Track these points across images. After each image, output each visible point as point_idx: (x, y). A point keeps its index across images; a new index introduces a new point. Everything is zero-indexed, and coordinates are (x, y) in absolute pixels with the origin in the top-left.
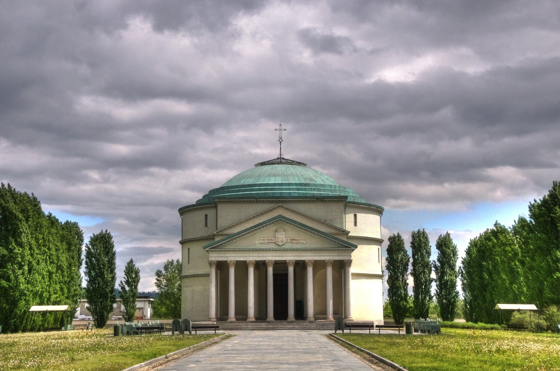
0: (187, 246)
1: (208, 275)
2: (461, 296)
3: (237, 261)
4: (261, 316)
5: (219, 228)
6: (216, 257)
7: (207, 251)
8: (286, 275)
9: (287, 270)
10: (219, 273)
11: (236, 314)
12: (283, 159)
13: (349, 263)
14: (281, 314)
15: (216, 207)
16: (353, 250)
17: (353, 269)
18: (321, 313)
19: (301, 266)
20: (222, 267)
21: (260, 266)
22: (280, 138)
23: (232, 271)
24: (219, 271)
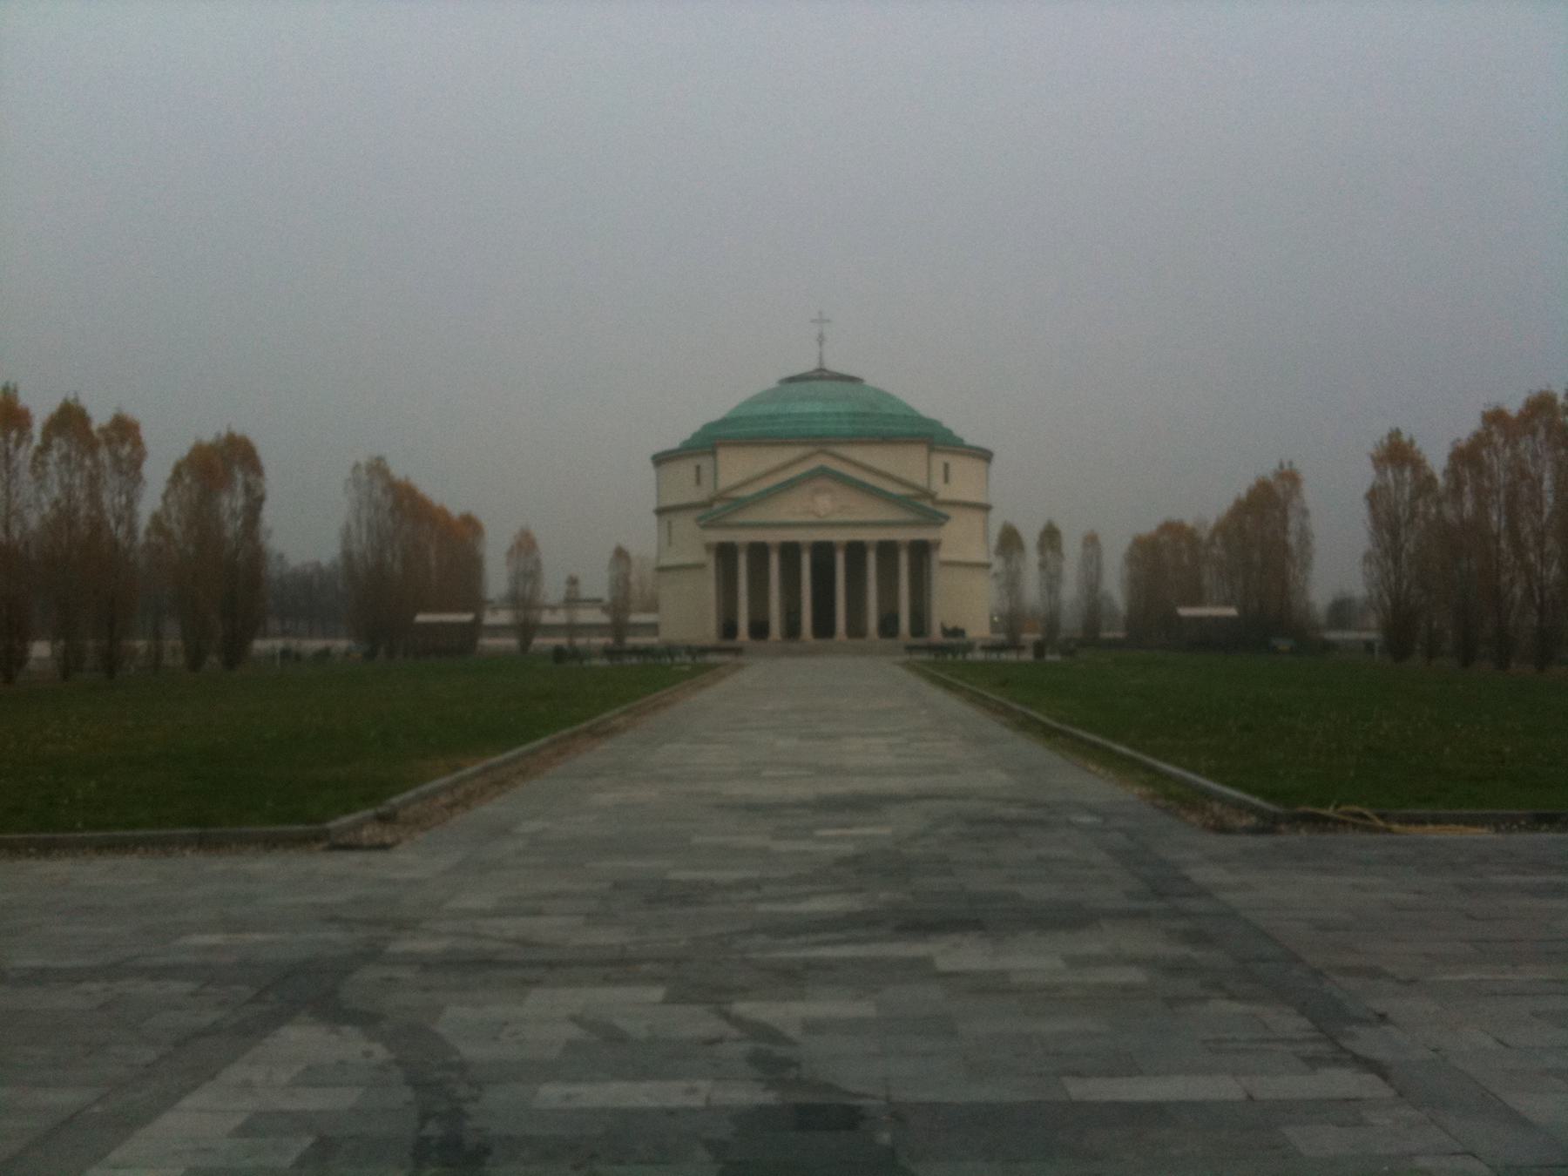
21: (790, 552)
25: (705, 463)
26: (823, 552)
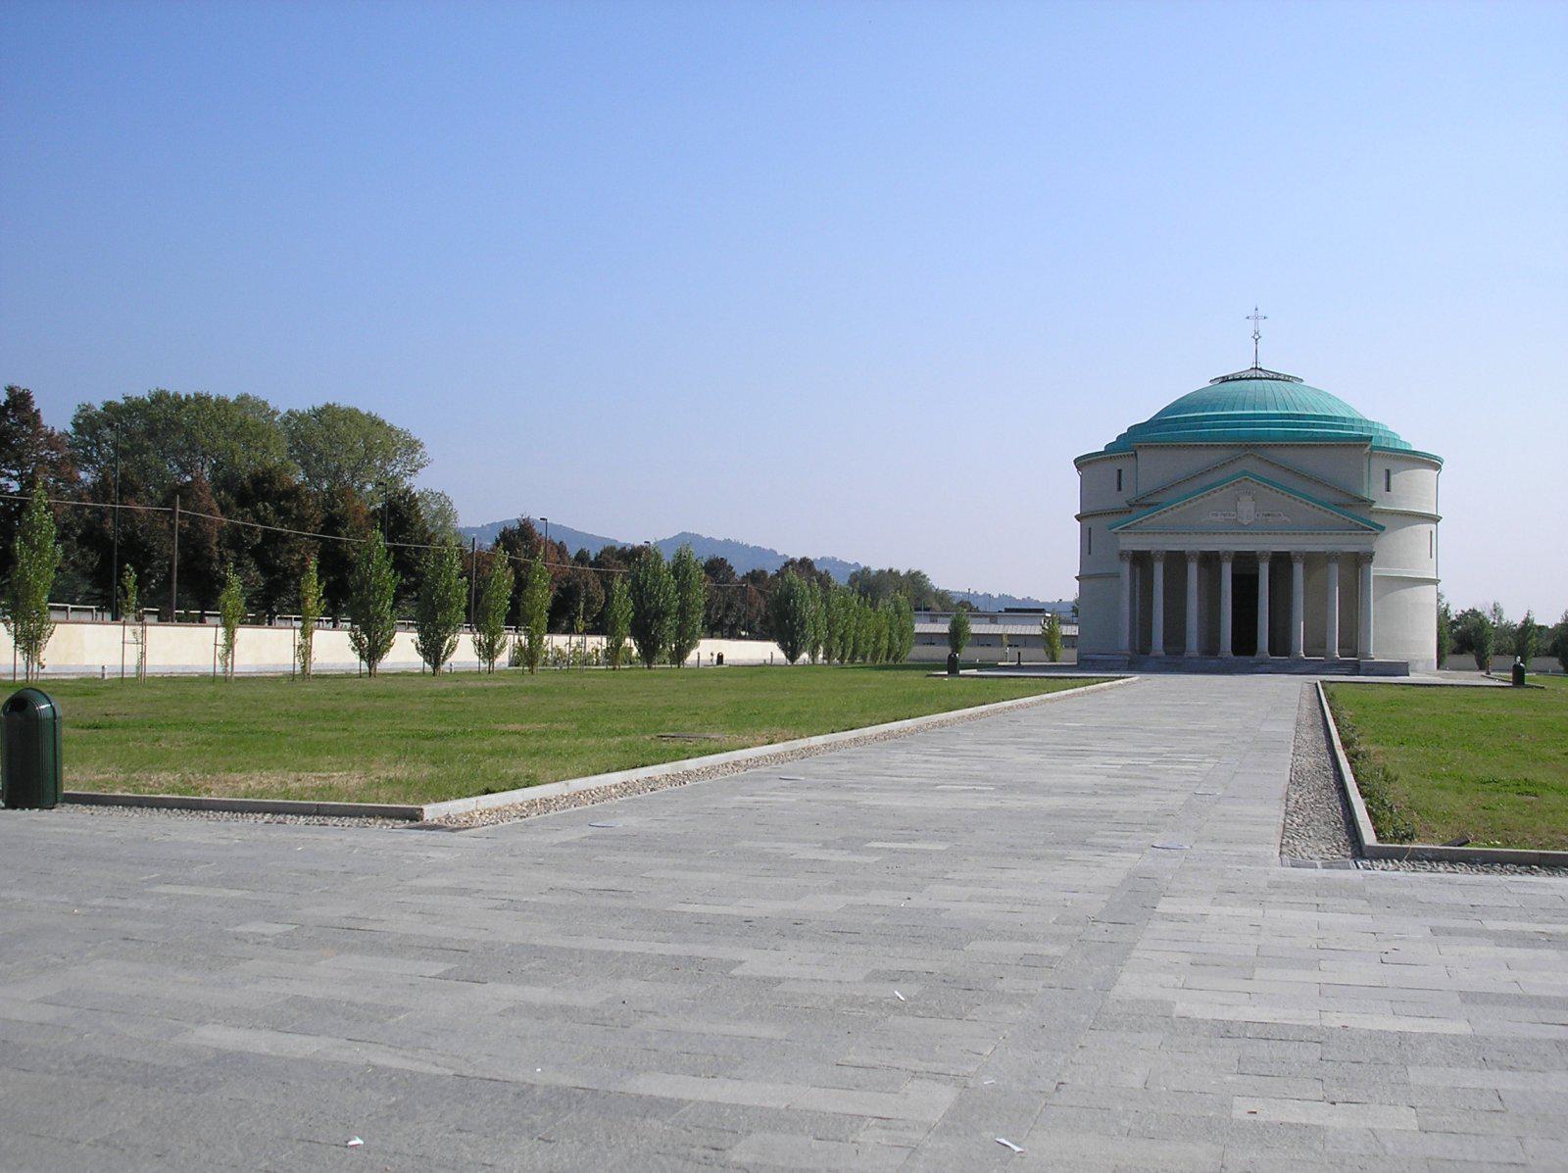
0: (1090, 522)
1: (1117, 576)
4: (1211, 647)
7: (1116, 533)
12: (1261, 369)
13: (1368, 557)
17: (1375, 570)
18: (1316, 644)
19: (1282, 562)
20: (1141, 561)
21: (1210, 561)
23: (1159, 570)
24: (1138, 570)
25: (1126, 465)
26: (1244, 564)
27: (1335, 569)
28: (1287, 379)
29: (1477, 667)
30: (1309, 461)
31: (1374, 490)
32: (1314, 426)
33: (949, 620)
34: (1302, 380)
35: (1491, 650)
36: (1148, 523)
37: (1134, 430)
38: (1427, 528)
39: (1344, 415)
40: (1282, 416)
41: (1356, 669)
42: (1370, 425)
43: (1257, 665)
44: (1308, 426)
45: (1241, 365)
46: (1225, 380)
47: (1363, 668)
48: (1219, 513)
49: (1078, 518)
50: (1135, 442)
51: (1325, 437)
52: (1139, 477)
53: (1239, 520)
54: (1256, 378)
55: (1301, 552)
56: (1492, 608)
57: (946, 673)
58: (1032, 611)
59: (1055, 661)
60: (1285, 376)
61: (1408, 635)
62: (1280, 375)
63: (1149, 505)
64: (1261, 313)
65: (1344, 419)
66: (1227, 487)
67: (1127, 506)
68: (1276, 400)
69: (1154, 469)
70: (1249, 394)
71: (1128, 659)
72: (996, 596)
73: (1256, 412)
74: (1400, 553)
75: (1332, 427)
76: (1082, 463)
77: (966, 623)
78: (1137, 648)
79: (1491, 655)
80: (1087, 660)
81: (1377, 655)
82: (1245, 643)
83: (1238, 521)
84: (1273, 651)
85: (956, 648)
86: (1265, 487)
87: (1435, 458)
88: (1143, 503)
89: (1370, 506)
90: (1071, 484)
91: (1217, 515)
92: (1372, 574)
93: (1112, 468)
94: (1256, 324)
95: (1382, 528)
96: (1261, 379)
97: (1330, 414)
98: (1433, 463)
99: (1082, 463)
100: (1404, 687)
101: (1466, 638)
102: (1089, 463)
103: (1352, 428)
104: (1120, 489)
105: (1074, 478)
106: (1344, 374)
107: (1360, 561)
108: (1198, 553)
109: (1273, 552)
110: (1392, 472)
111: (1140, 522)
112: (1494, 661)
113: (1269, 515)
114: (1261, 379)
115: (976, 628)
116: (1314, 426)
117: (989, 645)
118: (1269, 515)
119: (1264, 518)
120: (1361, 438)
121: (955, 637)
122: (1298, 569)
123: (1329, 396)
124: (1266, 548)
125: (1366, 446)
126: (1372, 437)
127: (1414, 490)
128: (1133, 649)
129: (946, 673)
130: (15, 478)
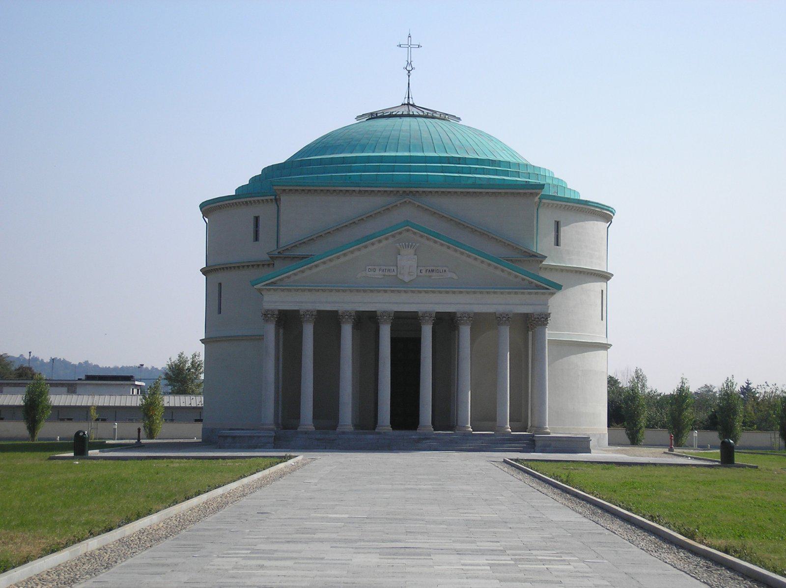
0: (220, 277)
1: (260, 338)
2: (56, 455)
3: (319, 312)
4: (366, 420)
5: (283, 242)
6: (279, 301)
7: (260, 290)
8: (417, 342)
9: (419, 330)
10: (281, 335)
11: (316, 416)
12: (413, 105)
13: (542, 319)
14: (405, 417)
15: (277, 201)
16: (553, 294)
17: (550, 334)
18: (486, 416)
19: (446, 324)
20: (288, 322)
21: (366, 322)
22: (409, 64)
23: (308, 331)
24: (281, 331)
25: (266, 212)
26: (406, 329)
27: (505, 333)
28: (444, 117)
29: (628, 441)
30: (451, 205)
31: (543, 244)
32: (476, 171)
33: (25, 389)
34: (459, 119)
35: (643, 421)
36: (297, 278)
37: (271, 172)
38: (597, 286)
39: (507, 159)
40: (440, 160)
41: (531, 445)
42: (536, 171)
43: (419, 441)
44: (470, 171)
45: (392, 100)
46: (373, 116)
47: (539, 444)
48: (377, 268)
49: (205, 271)
50: (272, 187)
51: (491, 184)
52: (269, 225)
53: (400, 277)
54: (409, 116)
55: (272, 311)
56: (634, 375)
57: (72, 454)
58: (120, 379)
59: (152, 438)
60: (441, 113)
61: (579, 407)
62: (435, 112)
63: (303, 258)
64: (414, 41)
65: (509, 164)
66: (387, 239)
67: (269, 259)
68: (434, 141)
69: (300, 217)
70: (402, 133)
71: (273, 434)
72: (89, 363)
73: (412, 154)
74: (572, 314)
75: (496, 172)
76: (209, 208)
77: (42, 394)
78: (280, 422)
79: (644, 429)
80: (226, 437)
81: (554, 428)
82: (405, 417)
83: (394, 277)
84: (396, 424)
85: (33, 427)
86: (428, 239)
87: (608, 208)
88: (287, 256)
89: (541, 262)
90: (197, 229)
91: (374, 270)
92: (547, 338)
93: (246, 215)
94: (409, 54)
95: (559, 287)
96: (413, 116)
97: (492, 158)
98: (603, 214)
99: (209, 208)
100: (607, 466)
101: (628, 411)
102: (220, 207)
103: (518, 174)
104: (256, 239)
105: (199, 226)
106: (509, 112)
107: (532, 324)
108: (353, 314)
109: (437, 313)
110: (561, 224)
111: (288, 277)
112: (647, 434)
113: (433, 271)
114: (413, 116)
115: (58, 399)
116: (476, 171)
117: (71, 419)
118: (433, 271)
119: (428, 274)
120: (528, 185)
121: (32, 411)
122: (465, 332)
123: (490, 137)
124: (310, 307)
125: (537, 194)
126: (544, 185)
127: (582, 245)
128: (276, 423)
129: (72, 454)
130: (416, 244)
